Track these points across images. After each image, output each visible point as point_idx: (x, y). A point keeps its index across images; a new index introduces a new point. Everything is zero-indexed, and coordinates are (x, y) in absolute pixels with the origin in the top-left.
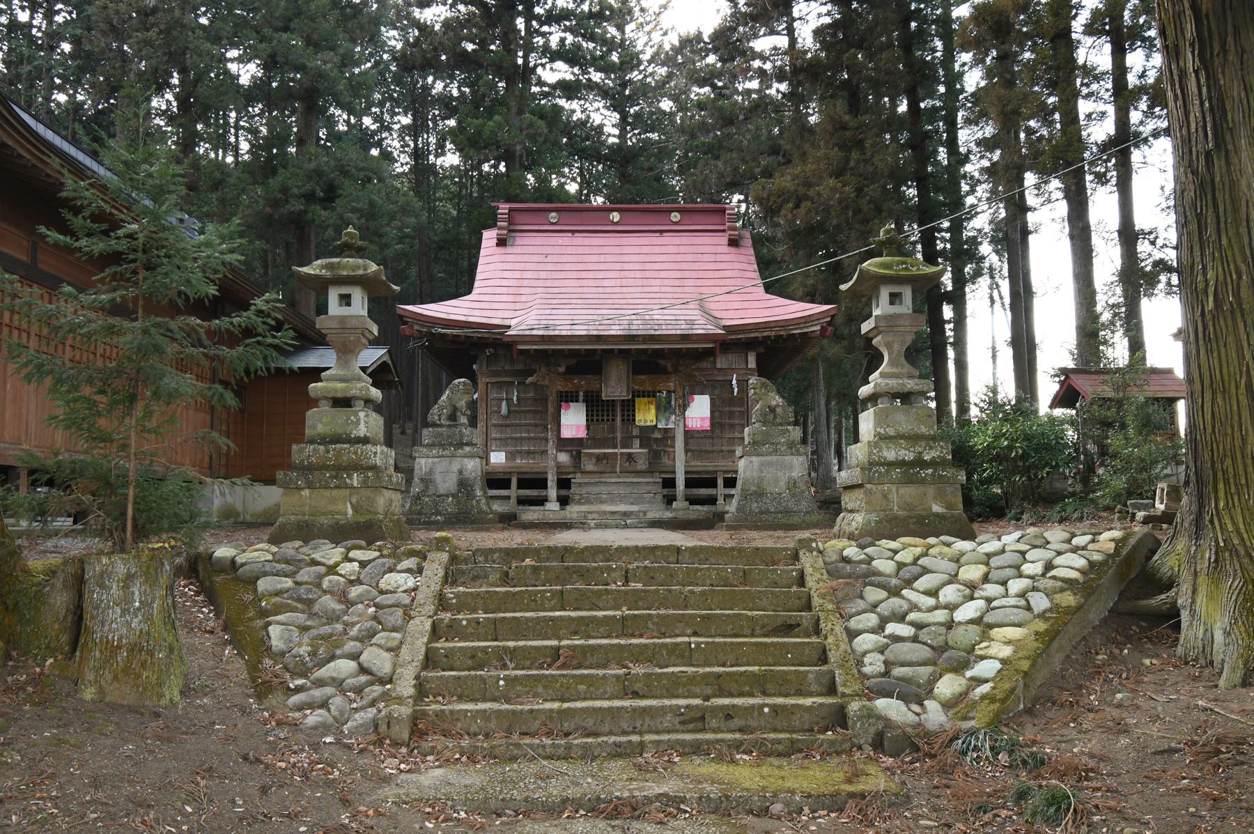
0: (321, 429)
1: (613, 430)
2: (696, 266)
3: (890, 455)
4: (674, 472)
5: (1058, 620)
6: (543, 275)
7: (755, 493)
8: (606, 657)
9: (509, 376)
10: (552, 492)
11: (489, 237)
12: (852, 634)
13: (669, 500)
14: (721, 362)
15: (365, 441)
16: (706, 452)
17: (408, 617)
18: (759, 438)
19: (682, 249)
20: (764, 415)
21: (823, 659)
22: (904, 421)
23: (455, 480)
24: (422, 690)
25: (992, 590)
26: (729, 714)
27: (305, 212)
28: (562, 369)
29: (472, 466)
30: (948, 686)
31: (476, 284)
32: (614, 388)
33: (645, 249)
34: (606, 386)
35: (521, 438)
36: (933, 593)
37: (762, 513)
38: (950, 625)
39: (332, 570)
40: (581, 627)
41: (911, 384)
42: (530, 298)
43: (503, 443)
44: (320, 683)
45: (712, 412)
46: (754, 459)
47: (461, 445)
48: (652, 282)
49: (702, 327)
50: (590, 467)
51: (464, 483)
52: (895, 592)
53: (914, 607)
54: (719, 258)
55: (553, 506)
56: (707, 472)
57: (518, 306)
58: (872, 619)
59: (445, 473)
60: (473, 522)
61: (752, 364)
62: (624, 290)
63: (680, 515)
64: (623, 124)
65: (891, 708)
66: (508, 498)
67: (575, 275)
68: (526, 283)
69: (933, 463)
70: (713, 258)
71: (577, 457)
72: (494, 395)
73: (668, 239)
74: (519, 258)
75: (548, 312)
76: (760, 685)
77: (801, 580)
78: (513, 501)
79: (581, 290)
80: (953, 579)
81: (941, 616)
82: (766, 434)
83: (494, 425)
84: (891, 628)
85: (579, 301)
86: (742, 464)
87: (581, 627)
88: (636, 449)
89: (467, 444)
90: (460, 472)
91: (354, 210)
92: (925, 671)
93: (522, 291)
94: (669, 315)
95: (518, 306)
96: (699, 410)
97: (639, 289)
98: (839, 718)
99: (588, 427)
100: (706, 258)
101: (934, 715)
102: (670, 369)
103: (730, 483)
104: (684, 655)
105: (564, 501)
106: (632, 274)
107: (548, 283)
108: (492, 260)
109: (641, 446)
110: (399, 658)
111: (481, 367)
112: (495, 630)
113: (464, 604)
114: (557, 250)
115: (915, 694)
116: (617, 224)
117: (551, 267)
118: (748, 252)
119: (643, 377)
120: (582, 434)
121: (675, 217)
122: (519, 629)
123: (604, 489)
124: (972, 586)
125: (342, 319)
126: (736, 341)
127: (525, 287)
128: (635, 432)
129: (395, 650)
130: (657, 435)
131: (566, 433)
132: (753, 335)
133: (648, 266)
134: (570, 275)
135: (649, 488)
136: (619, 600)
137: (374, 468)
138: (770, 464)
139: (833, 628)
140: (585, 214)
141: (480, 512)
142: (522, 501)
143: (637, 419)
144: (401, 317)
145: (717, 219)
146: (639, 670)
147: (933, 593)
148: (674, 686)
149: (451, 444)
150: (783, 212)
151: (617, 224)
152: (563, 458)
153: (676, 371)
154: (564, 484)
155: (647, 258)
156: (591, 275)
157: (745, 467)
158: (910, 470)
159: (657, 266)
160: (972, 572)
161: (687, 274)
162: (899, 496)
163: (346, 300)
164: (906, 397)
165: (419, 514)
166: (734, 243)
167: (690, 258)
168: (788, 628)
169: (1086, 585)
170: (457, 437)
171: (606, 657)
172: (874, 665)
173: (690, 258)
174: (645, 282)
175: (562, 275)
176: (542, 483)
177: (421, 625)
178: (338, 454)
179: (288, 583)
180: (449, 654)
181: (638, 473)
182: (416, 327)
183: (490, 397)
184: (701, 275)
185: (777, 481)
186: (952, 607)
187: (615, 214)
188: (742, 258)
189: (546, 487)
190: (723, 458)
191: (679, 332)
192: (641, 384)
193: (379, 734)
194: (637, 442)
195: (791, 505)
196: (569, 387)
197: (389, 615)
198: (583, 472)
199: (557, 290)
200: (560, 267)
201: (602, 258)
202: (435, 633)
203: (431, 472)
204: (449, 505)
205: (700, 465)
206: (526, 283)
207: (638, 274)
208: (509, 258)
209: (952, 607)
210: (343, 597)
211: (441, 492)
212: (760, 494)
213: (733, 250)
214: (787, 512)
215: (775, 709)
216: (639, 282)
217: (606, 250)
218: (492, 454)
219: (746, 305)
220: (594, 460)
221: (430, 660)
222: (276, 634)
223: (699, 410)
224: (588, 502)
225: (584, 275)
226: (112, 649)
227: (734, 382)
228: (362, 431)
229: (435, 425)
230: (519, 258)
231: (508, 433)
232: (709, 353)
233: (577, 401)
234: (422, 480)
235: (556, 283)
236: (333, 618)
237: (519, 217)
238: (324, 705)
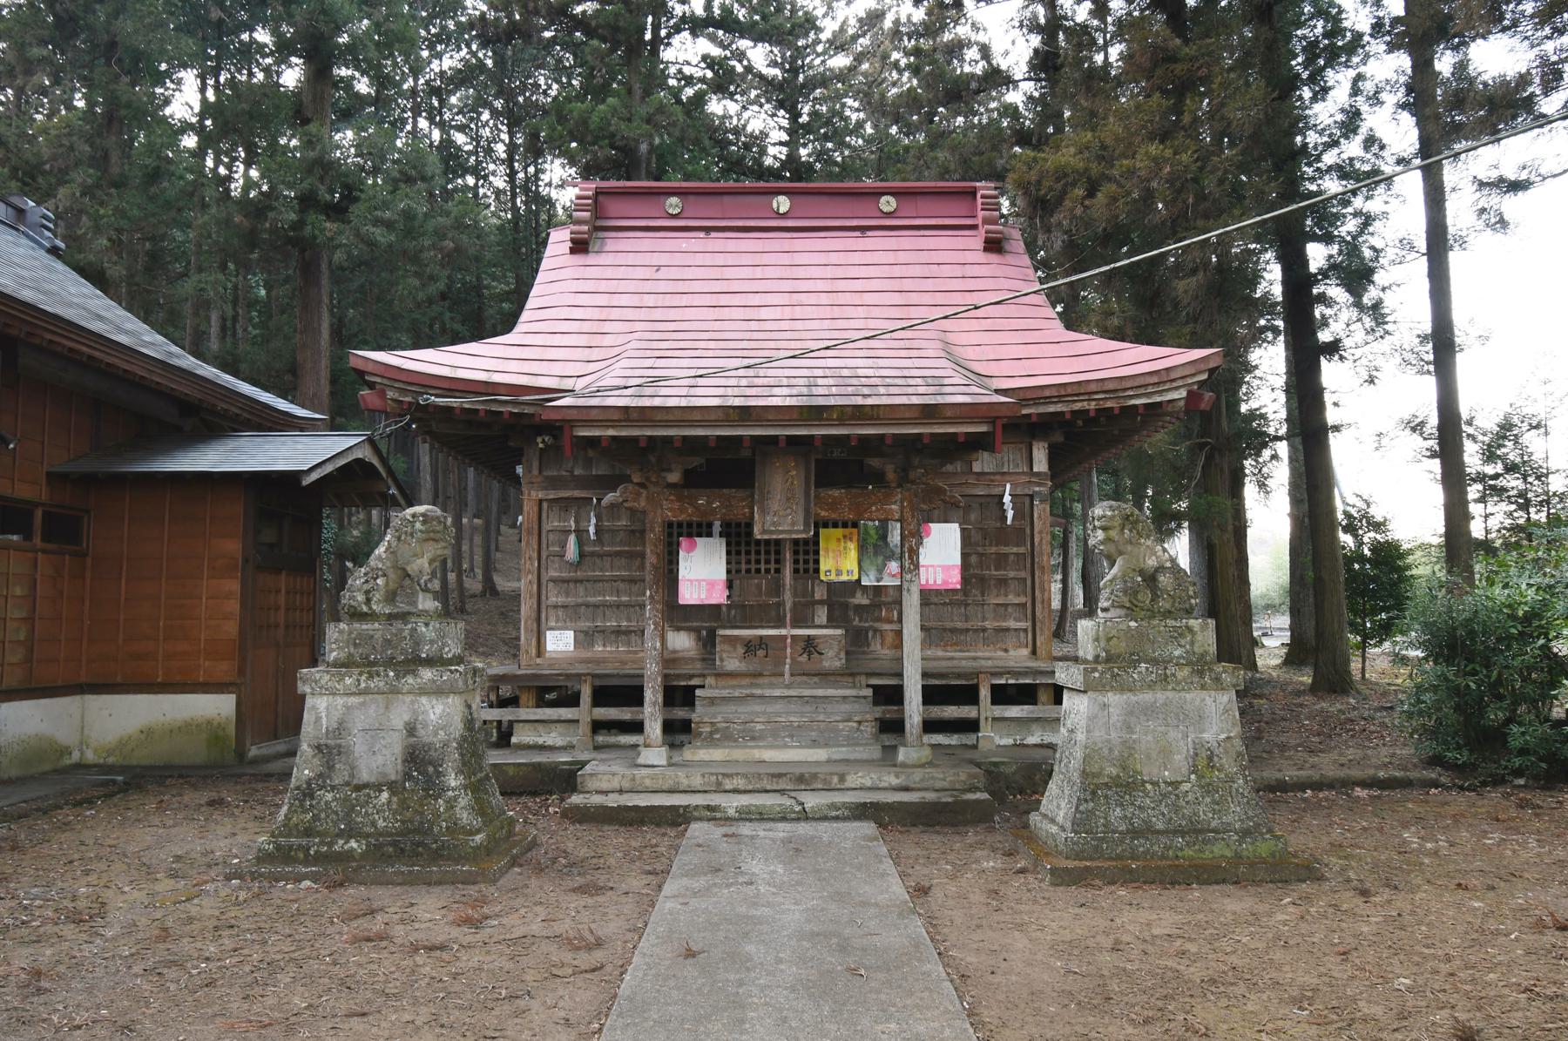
1: (777, 589)
2: (929, 285)
4: (900, 675)
6: (650, 300)
7: (1116, 782)
9: (583, 487)
10: (652, 714)
14: (983, 463)
16: (953, 631)
18: (1121, 647)
19: (902, 257)
20: (1132, 592)
23: (398, 749)
28: (674, 477)
31: (525, 316)
34: (763, 511)
35: (605, 605)
37: (1135, 833)
42: (621, 339)
43: (570, 615)
45: (964, 556)
46: (1112, 698)
47: (414, 662)
48: (850, 312)
51: (419, 760)
54: (969, 271)
56: (959, 676)
57: (595, 354)
59: (375, 731)
60: (436, 856)
61: (1041, 463)
62: (799, 325)
64: (796, 132)
67: (709, 300)
68: (615, 314)
70: (958, 271)
71: (708, 642)
72: (553, 523)
73: (874, 241)
74: (609, 273)
75: (649, 363)
79: (717, 325)
82: (1140, 636)
83: (554, 581)
85: (712, 345)
88: (823, 632)
89: (430, 662)
90: (411, 730)
91: (377, 222)
93: (607, 327)
94: (889, 366)
95: (595, 354)
96: (942, 551)
97: (826, 324)
99: (730, 585)
100: (947, 271)
102: (891, 475)
105: (677, 731)
106: (812, 299)
107: (658, 314)
109: (832, 622)
111: (528, 470)
114: (679, 259)
116: (784, 216)
117: (662, 286)
119: (836, 493)
120: (719, 597)
121: (888, 203)
126: (1025, 421)
127: (609, 324)
128: (820, 593)
130: (861, 599)
132: (1052, 409)
133: (841, 285)
134: (697, 300)
135: (846, 707)
138: (1149, 711)
140: (726, 199)
143: (823, 567)
144: (361, 373)
145: (960, 206)
149: (390, 663)
150: (1067, 203)
151: (784, 216)
152: (681, 642)
153: (904, 480)
154: (679, 695)
155: (840, 272)
159: (858, 285)
161: (914, 298)
165: (308, 832)
166: (994, 245)
170: (407, 645)
174: (837, 312)
175: (685, 300)
176: (631, 694)
181: (826, 676)
182: (390, 394)
183: (546, 527)
185: (1166, 752)
187: (782, 198)
189: (639, 702)
190: (986, 642)
191: (915, 400)
192: (833, 506)
194: (822, 615)
195: (1204, 813)
199: (672, 326)
200: (681, 287)
201: (758, 273)
203: (340, 729)
204: (381, 812)
206: (615, 314)
207: (824, 299)
211: (365, 776)
212: (1128, 785)
213: (993, 258)
214: (1195, 831)
216: (827, 312)
217: (766, 259)
218: (550, 635)
219: (1033, 351)
220: (741, 650)
223: (942, 551)
227: (1007, 499)
229: (357, 615)
230: (609, 273)
231: (580, 595)
232: (977, 444)
233: (710, 535)
234: (318, 748)
235: (672, 314)
237: (613, 206)
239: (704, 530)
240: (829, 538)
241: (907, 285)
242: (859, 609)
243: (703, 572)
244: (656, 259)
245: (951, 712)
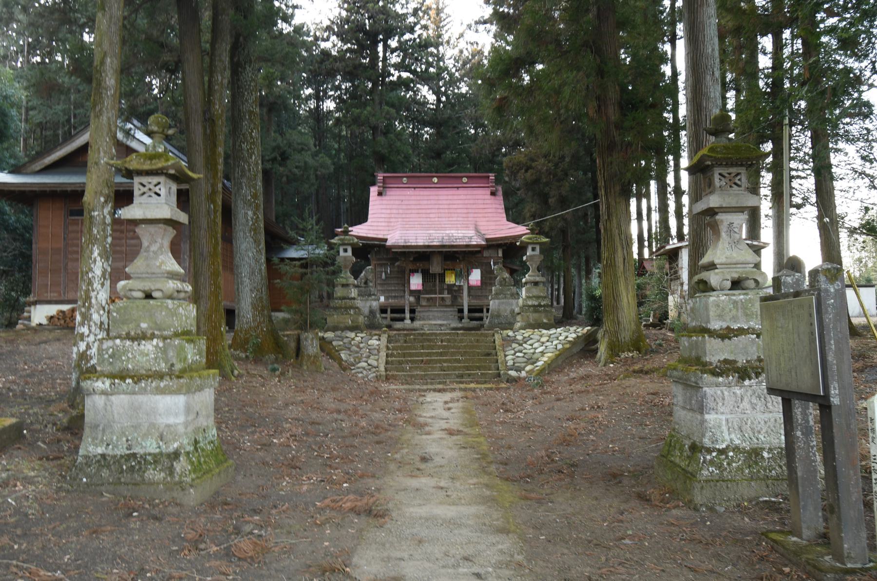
0: (339, 294)
1: (435, 286)
2: (474, 206)
3: (530, 303)
5: (564, 350)
8: (436, 361)
10: (408, 315)
11: (374, 190)
12: (506, 356)
13: (461, 318)
15: (354, 299)
17: (379, 352)
19: (468, 197)
21: (497, 362)
22: (535, 291)
24: (386, 370)
25: (548, 344)
26: (469, 375)
27: (271, 169)
28: (411, 259)
29: (375, 304)
30: (528, 368)
31: (369, 216)
32: (435, 268)
33: (450, 197)
36: (532, 345)
38: (533, 353)
39: (353, 339)
40: (428, 355)
41: (538, 279)
44: (359, 368)
47: (370, 295)
49: (476, 241)
50: (424, 303)
51: (372, 312)
52: (521, 345)
53: (525, 349)
54: (486, 202)
55: (408, 321)
58: (513, 352)
61: (500, 254)
63: (466, 325)
65: (513, 373)
66: (386, 318)
69: (544, 306)
71: (418, 299)
72: (378, 269)
76: (479, 368)
77: (494, 342)
78: (389, 319)
80: (539, 341)
81: (532, 351)
84: (518, 354)
86: (491, 302)
87: (428, 355)
88: (446, 295)
91: (297, 167)
92: (523, 365)
96: (476, 276)
98: (499, 375)
101: (523, 374)
103: (488, 311)
104: (458, 361)
105: (412, 319)
108: (376, 204)
110: (380, 362)
112: (404, 355)
113: (394, 348)
114: (407, 197)
115: (519, 370)
117: (404, 207)
118: (500, 198)
120: (420, 288)
122: (411, 355)
123: (431, 314)
124: (543, 343)
125: (345, 258)
126: (492, 244)
128: (445, 287)
129: (377, 360)
130: (456, 288)
131: (413, 287)
136: (440, 347)
137: (357, 308)
139: (501, 355)
141: (379, 323)
142: (393, 319)
146: (445, 365)
147: (532, 345)
148: (455, 369)
152: (412, 299)
154: (412, 311)
156: (424, 211)
157: (493, 304)
158: (536, 308)
159: (455, 206)
160: (544, 339)
161: (470, 211)
162: (532, 317)
163: (345, 251)
164: (536, 284)
166: (493, 194)
167: (471, 202)
168: (488, 355)
169: (573, 343)
171: (436, 361)
172: (510, 363)
173: (471, 202)
176: (402, 311)
177: (383, 354)
178: (346, 303)
179: (341, 343)
180: (392, 361)
181: (446, 306)
184: (477, 211)
185: (506, 311)
186: (535, 349)
188: (497, 202)
193: (378, 378)
194: (446, 292)
196: (414, 267)
198: (422, 306)
201: (429, 202)
202: (387, 356)
205: (475, 302)
208: (384, 202)
209: (535, 349)
210: (358, 347)
213: (493, 197)
215: (482, 374)
217: (431, 197)
221: (387, 363)
222: (343, 356)
223: (476, 276)
224: (424, 319)
225: (420, 211)
226: (309, 356)
228: (353, 295)
231: (386, 287)
236: (357, 352)
237: (388, 181)
238: (361, 372)
239: (417, 271)
240: (447, 273)
241: (469, 206)
242: (455, 291)
243: (416, 282)
244: (401, 198)
245: (477, 315)
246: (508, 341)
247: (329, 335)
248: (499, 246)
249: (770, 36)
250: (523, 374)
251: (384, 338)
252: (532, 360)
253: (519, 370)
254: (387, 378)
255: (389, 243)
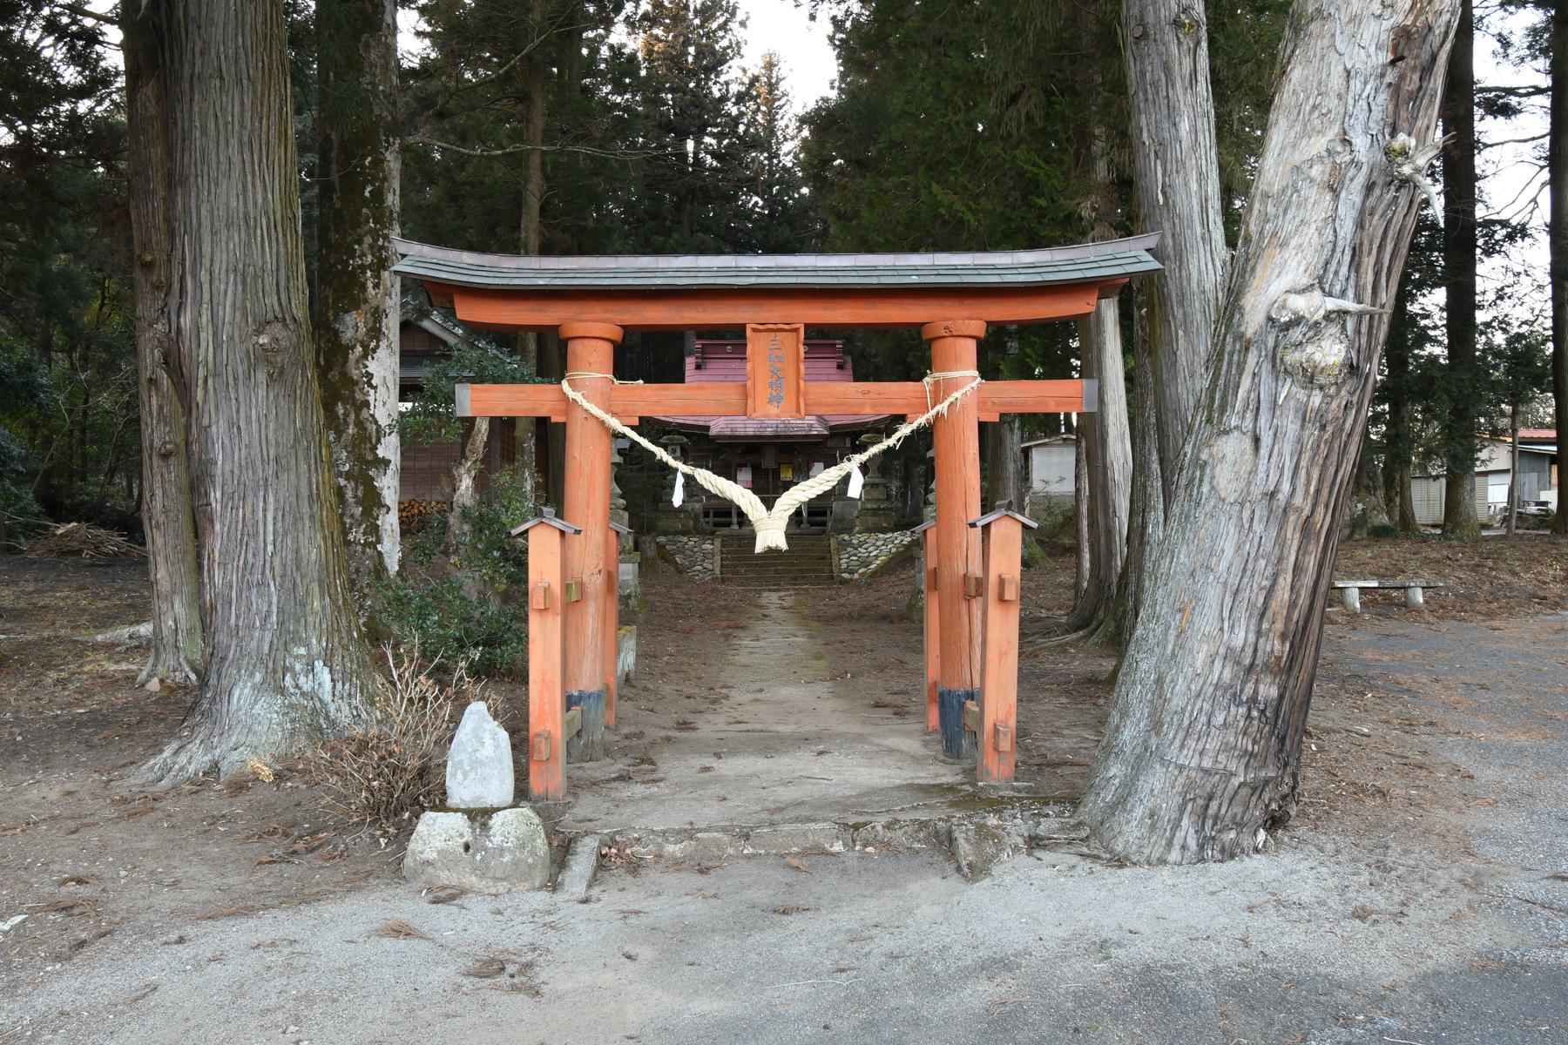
10: (735, 520)
32: (768, 462)
55: (735, 527)
65: (846, 575)
101: (856, 576)
112: (739, 559)
115: (852, 572)
142: (716, 525)
158: (875, 512)
162: (871, 520)
166: (840, 367)
177: (718, 558)
193: (714, 580)
197: (706, 556)
239: (745, 466)
246: (844, 545)
247: (662, 539)
248: (846, 434)
249: (759, 549)
250: (856, 576)
251: (718, 542)
252: (865, 563)
253: (852, 572)
254: (723, 581)
255: (713, 432)
